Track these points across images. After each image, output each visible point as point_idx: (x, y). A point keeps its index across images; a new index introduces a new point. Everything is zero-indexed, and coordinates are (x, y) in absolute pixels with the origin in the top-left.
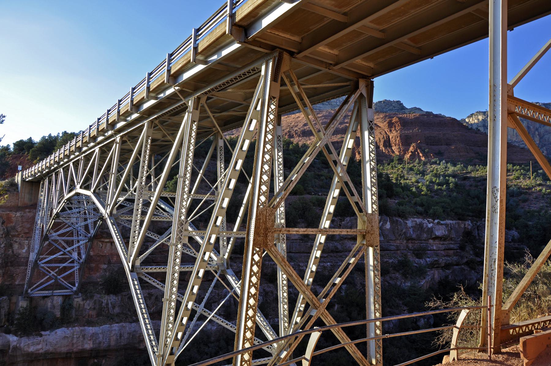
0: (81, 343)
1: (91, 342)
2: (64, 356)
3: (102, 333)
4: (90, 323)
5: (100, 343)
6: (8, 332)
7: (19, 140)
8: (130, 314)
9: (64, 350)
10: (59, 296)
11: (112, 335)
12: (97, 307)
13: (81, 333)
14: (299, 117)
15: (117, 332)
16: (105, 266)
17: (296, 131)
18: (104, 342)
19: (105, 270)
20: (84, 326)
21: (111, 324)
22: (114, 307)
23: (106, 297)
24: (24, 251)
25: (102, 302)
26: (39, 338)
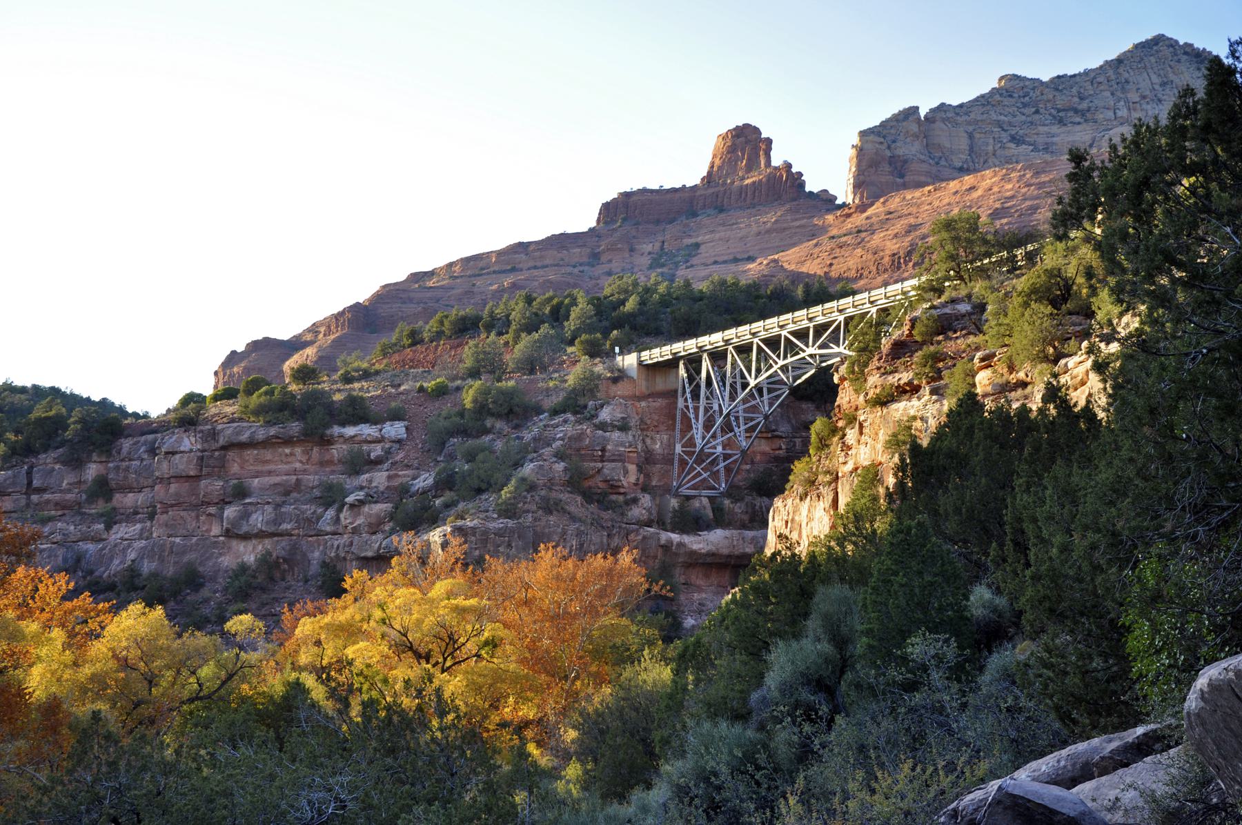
1: (752, 546)
2: (723, 561)
9: (725, 551)
12: (750, 510)
14: (973, 188)
16: (748, 467)
19: (748, 471)
23: (759, 499)
24: (657, 446)
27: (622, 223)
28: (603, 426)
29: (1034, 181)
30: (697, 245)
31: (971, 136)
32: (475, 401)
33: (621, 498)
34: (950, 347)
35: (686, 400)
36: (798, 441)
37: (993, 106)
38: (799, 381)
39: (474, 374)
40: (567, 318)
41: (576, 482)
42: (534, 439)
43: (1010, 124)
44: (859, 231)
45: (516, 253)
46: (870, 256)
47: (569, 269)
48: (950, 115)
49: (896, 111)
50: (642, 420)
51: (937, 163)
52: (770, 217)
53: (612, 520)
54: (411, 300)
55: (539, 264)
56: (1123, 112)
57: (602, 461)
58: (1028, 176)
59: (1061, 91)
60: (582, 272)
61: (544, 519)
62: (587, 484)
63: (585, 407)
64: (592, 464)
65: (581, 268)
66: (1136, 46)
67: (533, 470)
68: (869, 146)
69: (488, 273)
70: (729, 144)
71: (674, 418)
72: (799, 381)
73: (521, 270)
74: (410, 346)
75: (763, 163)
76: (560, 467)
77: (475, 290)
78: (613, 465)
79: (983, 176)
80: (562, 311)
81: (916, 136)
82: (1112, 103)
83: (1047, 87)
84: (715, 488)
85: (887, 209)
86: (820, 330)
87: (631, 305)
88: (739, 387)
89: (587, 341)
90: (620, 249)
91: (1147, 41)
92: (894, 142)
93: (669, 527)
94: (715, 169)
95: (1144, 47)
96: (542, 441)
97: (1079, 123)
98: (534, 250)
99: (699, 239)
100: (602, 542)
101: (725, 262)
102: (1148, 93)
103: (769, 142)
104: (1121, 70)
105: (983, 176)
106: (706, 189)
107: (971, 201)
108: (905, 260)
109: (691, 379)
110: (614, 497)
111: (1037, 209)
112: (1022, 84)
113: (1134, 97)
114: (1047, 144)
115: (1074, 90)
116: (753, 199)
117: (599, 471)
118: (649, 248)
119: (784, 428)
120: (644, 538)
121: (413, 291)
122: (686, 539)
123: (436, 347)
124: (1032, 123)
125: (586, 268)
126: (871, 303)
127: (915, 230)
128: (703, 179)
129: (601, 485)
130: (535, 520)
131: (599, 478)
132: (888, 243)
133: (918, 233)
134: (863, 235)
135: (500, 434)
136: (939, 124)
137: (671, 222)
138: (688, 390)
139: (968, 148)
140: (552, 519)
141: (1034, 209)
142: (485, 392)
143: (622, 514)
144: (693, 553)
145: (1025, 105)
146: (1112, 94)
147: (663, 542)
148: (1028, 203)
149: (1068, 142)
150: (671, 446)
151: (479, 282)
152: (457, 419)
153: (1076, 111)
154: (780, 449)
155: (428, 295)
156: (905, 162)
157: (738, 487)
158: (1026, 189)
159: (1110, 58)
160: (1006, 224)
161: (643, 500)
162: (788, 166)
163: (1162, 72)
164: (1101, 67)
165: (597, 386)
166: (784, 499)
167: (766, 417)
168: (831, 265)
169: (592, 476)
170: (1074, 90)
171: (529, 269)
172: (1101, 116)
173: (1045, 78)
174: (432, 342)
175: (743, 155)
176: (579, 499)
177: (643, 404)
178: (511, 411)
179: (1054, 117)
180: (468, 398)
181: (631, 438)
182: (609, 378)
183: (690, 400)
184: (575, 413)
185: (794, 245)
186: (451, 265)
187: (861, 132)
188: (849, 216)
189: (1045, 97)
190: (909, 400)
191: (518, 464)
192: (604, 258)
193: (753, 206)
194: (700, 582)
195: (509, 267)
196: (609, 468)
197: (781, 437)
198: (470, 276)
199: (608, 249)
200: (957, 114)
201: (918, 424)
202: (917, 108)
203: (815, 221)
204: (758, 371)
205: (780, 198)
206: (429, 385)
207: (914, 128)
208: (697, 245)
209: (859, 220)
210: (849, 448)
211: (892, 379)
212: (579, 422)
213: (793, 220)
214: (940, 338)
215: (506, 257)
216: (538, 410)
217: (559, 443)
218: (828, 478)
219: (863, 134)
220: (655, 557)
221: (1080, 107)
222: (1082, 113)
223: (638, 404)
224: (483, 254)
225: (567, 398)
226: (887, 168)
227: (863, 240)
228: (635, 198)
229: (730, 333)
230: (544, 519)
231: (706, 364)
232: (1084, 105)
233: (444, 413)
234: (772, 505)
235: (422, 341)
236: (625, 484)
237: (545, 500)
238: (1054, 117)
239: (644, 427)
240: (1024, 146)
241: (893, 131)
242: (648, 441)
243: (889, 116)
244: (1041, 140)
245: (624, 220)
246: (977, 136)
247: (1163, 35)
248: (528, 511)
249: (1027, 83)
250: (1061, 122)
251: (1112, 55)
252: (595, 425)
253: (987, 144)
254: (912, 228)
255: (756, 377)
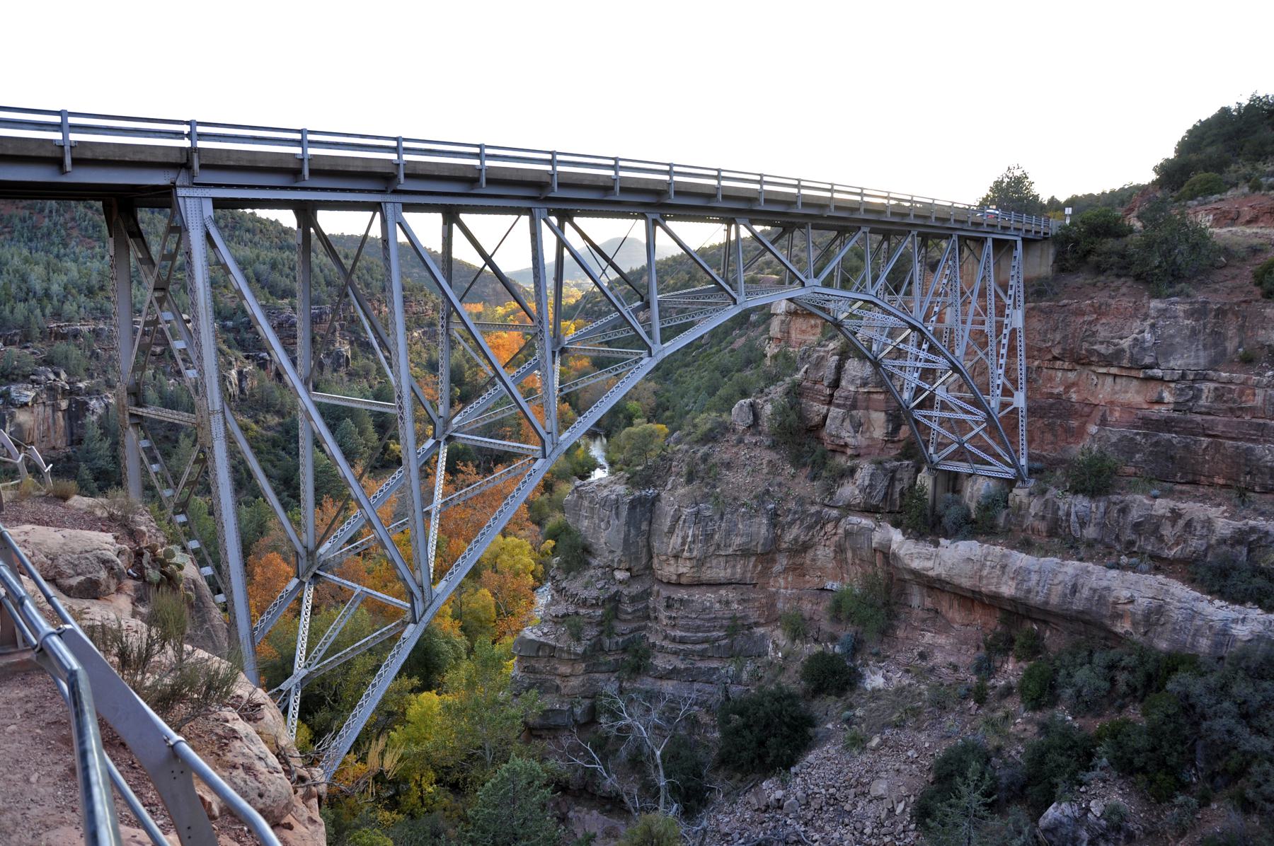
0: (995, 580)
1: (1013, 584)
3: (1039, 572)
4: (1027, 546)
5: (1029, 591)
6: (896, 525)
7: (1208, 111)
8: (1118, 548)
9: (966, 583)
10: (989, 477)
11: (1056, 581)
13: (1001, 560)
15: (1067, 579)
18: (1038, 592)
20: (1013, 548)
21: (1064, 559)
22: (1083, 524)
23: (1070, 497)
25: (1059, 508)
26: (932, 549)
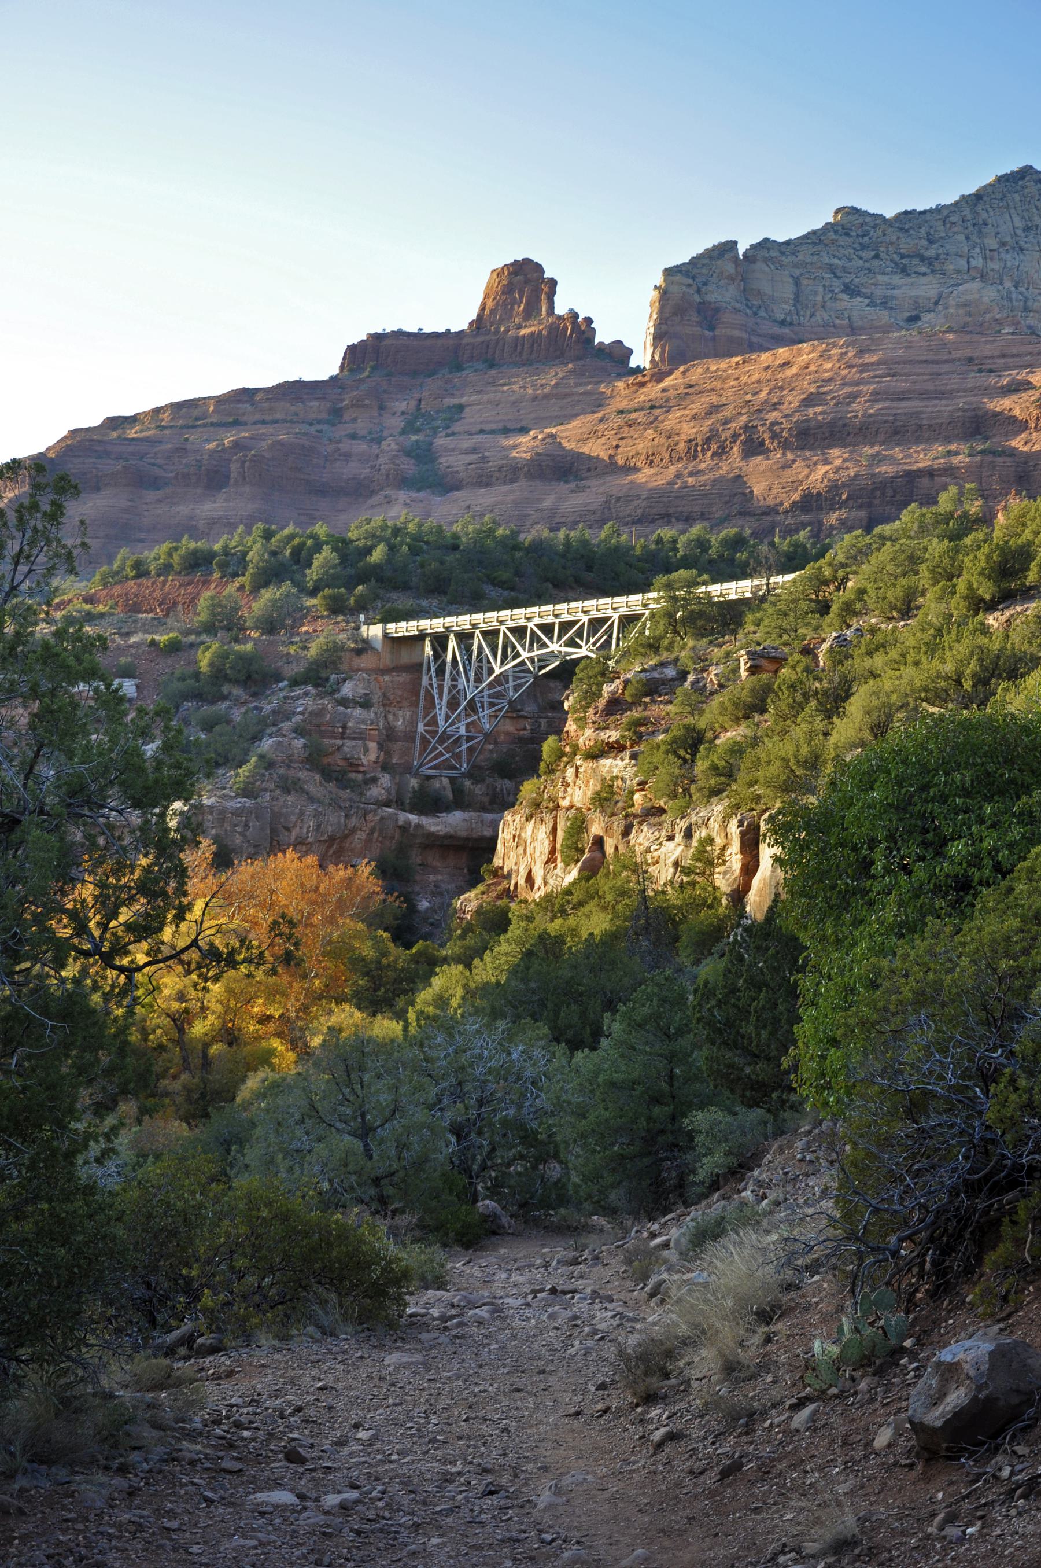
9: (463, 834)
14: (787, 364)
16: (491, 747)
17: (773, 424)
19: (491, 751)
23: (500, 781)
27: (371, 372)
28: (344, 702)
29: (857, 361)
30: (461, 408)
31: (797, 282)
32: (211, 664)
33: (360, 777)
34: (655, 711)
35: (430, 679)
36: (543, 721)
37: (826, 245)
38: (543, 672)
39: (209, 628)
40: (309, 565)
41: (314, 760)
42: (274, 712)
43: (844, 269)
44: (653, 407)
45: (239, 401)
46: (663, 440)
47: (305, 428)
48: (774, 254)
49: (710, 246)
50: (384, 695)
51: (755, 314)
52: (551, 377)
53: (351, 800)
54: (107, 454)
55: (268, 418)
56: (977, 262)
57: (343, 738)
58: (850, 354)
59: (907, 231)
60: (320, 431)
61: (282, 799)
62: (326, 760)
63: (327, 679)
64: (333, 741)
65: (319, 427)
66: (1000, 179)
67: (271, 746)
68: (674, 289)
69: (205, 426)
70: (505, 282)
71: (418, 695)
72: (543, 672)
73: (245, 424)
74: (134, 578)
75: (544, 309)
76: (299, 743)
77: (188, 447)
78: (353, 743)
79: (799, 350)
80: (304, 554)
81: (732, 279)
82: (966, 249)
83: (891, 226)
84: (455, 768)
85: (686, 380)
86: (565, 626)
87: (378, 555)
88: (485, 672)
89: (330, 597)
90: (367, 406)
91: (1012, 173)
92: (705, 284)
93: (407, 807)
94: (487, 312)
95: (1008, 180)
96: (282, 714)
97: (925, 274)
98: (261, 401)
99: (464, 400)
100: (339, 823)
101: (492, 432)
102: (1008, 239)
103: (553, 283)
104: (979, 209)
105: (799, 350)
106: (474, 337)
107: (783, 380)
108: (703, 449)
109: (437, 656)
110: (353, 775)
111: (856, 397)
112: (861, 220)
113: (992, 243)
114: (885, 297)
115: (923, 231)
116: (531, 353)
117: (339, 748)
118: (402, 406)
119: (530, 708)
120: (382, 818)
121: (111, 442)
122: (425, 821)
123: (164, 583)
124: (869, 270)
125: (325, 427)
126: (614, 609)
127: (717, 412)
128: (471, 324)
129: (340, 763)
130: (273, 799)
131: (338, 756)
132: (685, 426)
133: (720, 416)
134: (657, 412)
135: (238, 702)
136: (760, 265)
137: (430, 376)
138: (433, 669)
139: (792, 296)
140: (290, 799)
141: (853, 397)
142: (223, 656)
143: (361, 794)
144: (430, 835)
145: (863, 247)
146: (967, 238)
147: (400, 823)
148: (847, 389)
149: (911, 297)
150: (413, 723)
151: (193, 437)
152: (191, 682)
153: (922, 259)
154: (525, 729)
155: (131, 449)
156: (717, 310)
157: (480, 768)
158: (846, 371)
159: (967, 193)
160: (821, 413)
161: (382, 780)
162: (574, 315)
163: (1026, 214)
164: (957, 203)
165: (340, 658)
166: (514, 814)
167: (510, 702)
168: (617, 447)
169: (332, 753)
170: (923, 231)
171: (255, 423)
172: (951, 267)
173: (889, 214)
174: (159, 576)
175: (521, 298)
176: (318, 777)
177: (387, 678)
178: (249, 677)
179: (896, 264)
180: (205, 660)
181: (372, 716)
182: (353, 649)
183: (434, 680)
184: (316, 686)
185: (576, 416)
186: (158, 410)
187: (666, 270)
188: (642, 384)
189: (887, 239)
190: (615, 758)
191: (256, 738)
192: (347, 417)
193: (528, 363)
194: (437, 864)
195: (230, 420)
196: (348, 745)
197: (526, 717)
198: (182, 427)
199: (353, 406)
200: (783, 253)
201: (620, 783)
202: (735, 243)
203: (602, 388)
204: (505, 656)
205: (562, 354)
206: (162, 638)
207: (730, 268)
208: (461, 408)
209: (653, 391)
210: (568, 785)
211: (604, 735)
212: (320, 696)
213: (576, 385)
214: (648, 699)
215: (227, 406)
216: (278, 678)
217: (299, 717)
218: (551, 805)
219: (668, 272)
220: (393, 838)
221: (927, 254)
222: (929, 261)
223: (381, 678)
224: (199, 400)
225: (309, 670)
226: (695, 317)
227: (656, 419)
228: (387, 342)
229: (478, 617)
230: (282, 799)
231: (452, 643)
232: (931, 252)
233: (177, 673)
234: (502, 818)
235: (146, 574)
236: (365, 762)
237: (283, 778)
238: (896, 264)
239: (386, 702)
240: (859, 299)
241: (704, 271)
242: (390, 717)
243: (701, 251)
244: (879, 292)
245: (374, 368)
246: (804, 282)
247: (1031, 167)
248: (266, 790)
249: (868, 219)
250: (904, 271)
251: (970, 189)
252: (337, 701)
253: (816, 293)
254: (714, 409)
255: (502, 663)
